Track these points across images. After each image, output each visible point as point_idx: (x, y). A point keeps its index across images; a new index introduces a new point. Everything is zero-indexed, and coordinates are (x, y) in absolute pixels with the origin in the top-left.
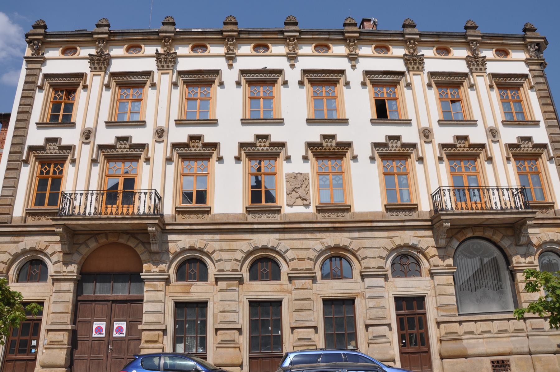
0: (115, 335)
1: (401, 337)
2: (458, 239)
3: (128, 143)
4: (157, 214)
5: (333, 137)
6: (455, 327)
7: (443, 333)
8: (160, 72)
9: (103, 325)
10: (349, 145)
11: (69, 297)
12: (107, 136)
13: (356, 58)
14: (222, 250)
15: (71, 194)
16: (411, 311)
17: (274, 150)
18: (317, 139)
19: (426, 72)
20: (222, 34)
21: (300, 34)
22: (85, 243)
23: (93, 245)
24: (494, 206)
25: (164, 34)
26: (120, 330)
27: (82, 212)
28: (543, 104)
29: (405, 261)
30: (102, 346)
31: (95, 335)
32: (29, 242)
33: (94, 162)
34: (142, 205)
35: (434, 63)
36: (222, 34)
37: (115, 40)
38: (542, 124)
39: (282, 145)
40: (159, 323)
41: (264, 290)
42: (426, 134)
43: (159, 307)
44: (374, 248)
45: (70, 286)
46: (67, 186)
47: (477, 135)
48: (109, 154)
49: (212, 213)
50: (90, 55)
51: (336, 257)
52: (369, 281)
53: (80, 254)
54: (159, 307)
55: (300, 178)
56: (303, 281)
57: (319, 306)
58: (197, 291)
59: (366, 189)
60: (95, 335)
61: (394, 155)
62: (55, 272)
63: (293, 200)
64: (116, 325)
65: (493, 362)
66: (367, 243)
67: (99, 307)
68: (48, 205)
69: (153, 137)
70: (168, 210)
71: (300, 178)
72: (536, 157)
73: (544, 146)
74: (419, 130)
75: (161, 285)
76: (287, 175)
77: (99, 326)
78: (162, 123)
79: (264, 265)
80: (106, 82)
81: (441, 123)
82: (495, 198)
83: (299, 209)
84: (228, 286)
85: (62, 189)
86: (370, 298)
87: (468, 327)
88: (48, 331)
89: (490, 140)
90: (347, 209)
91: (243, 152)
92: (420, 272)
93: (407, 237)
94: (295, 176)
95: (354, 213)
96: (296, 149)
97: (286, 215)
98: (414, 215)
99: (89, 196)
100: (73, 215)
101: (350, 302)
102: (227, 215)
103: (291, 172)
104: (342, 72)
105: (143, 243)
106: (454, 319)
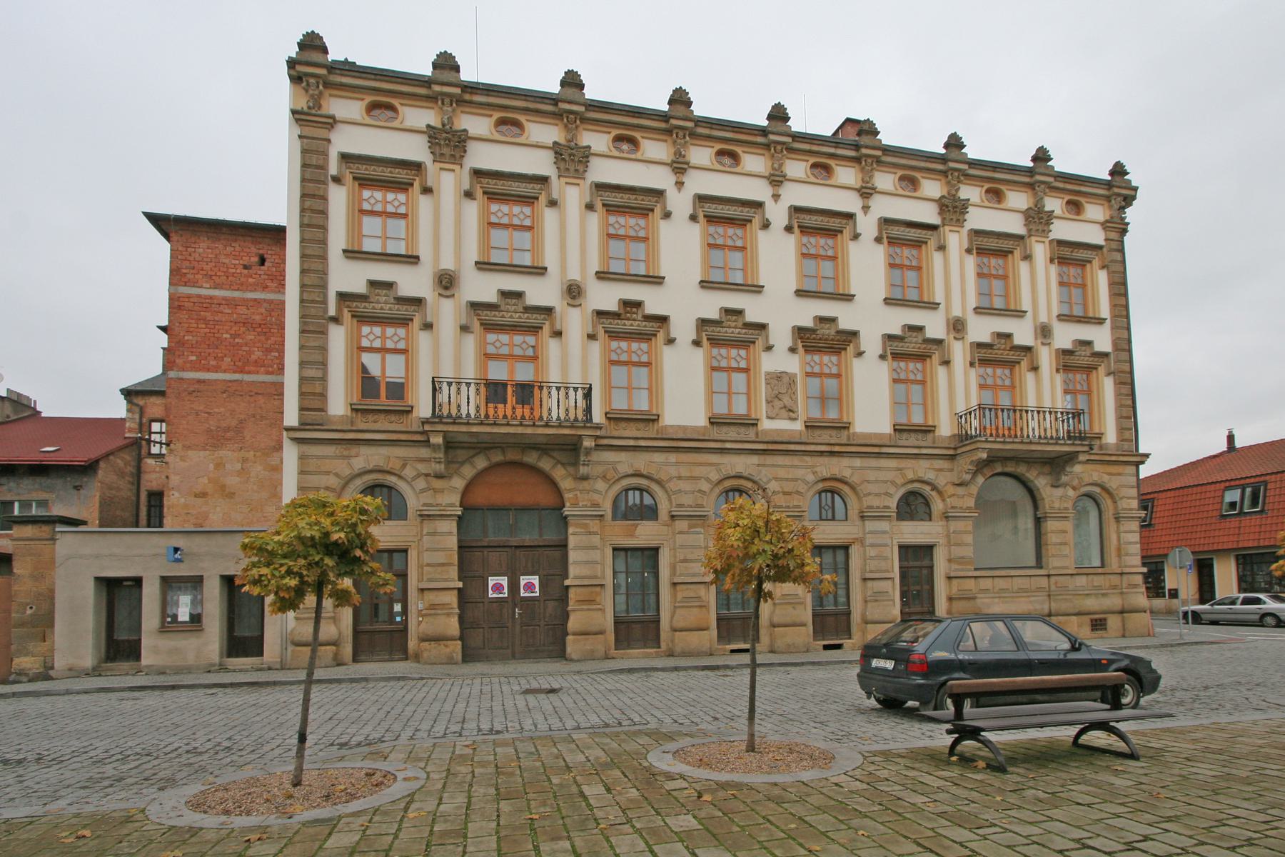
0: (523, 594)
1: (903, 594)
2: (984, 475)
3: (392, 294)
5: (833, 320)
6: (970, 584)
7: (955, 590)
8: (563, 180)
9: (504, 581)
10: (854, 334)
11: (453, 542)
13: (685, 170)
16: (916, 559)
18: (808, 323)
19: (589, 182)
20: (556, 105)
21: (330, 72)
22: (469, 460)
23: (481, 463)
24: (545, 415)
25: (567, 106)
26: (530, 587)
27: (562, 416)
28: (1115, 294)
29: (913, 504)
30: (505, 611)
31: (491, 595)
32: (366, 458)
34: (554, 407)
35: (982, 218)
36: (667, 121)
37: (471, 102)
38: (1108, 322)
39: (762, 327)
41: (915, 532)
42: (957, 326)
44: (882, 482)
45: (451, 526)
47: (1023, 334)
49: (661, 423)
50: (428, 126)
51: (634, 489)
52: (870, 525)
53: (463, 477)
55: (786, 380)
58: (645, 533)
59: (872, 403)
60: (491, 595)
61: (910, 351)
63: (776, 410)
64: (524, 580)
66: (872, 475)
67: (494, 557)
72: (1089, 369)
73: (1106, 355)
74: (948, 320)
75: (594, 525)
76: (767, 374)
77: (497, 585)
80: (966, 246)
81: (978, 310)
82: (1033, 424)
83: (783, 425)
84: (690, 527)
86: (872, 545)
87: (986, 584)
89: (1039, 341)
90: (651, 419)
91: (346, 310)
92: (930, 515)
93: (923, 469)
94: (779, 376)
95: (854, 434)
96: (781, 336)
97: (766, 432)
98: (651, 431)
100: (998, 436)
102: (685, 428)
103: (771, 369)
104: (659, 193)
106: (970, 574)
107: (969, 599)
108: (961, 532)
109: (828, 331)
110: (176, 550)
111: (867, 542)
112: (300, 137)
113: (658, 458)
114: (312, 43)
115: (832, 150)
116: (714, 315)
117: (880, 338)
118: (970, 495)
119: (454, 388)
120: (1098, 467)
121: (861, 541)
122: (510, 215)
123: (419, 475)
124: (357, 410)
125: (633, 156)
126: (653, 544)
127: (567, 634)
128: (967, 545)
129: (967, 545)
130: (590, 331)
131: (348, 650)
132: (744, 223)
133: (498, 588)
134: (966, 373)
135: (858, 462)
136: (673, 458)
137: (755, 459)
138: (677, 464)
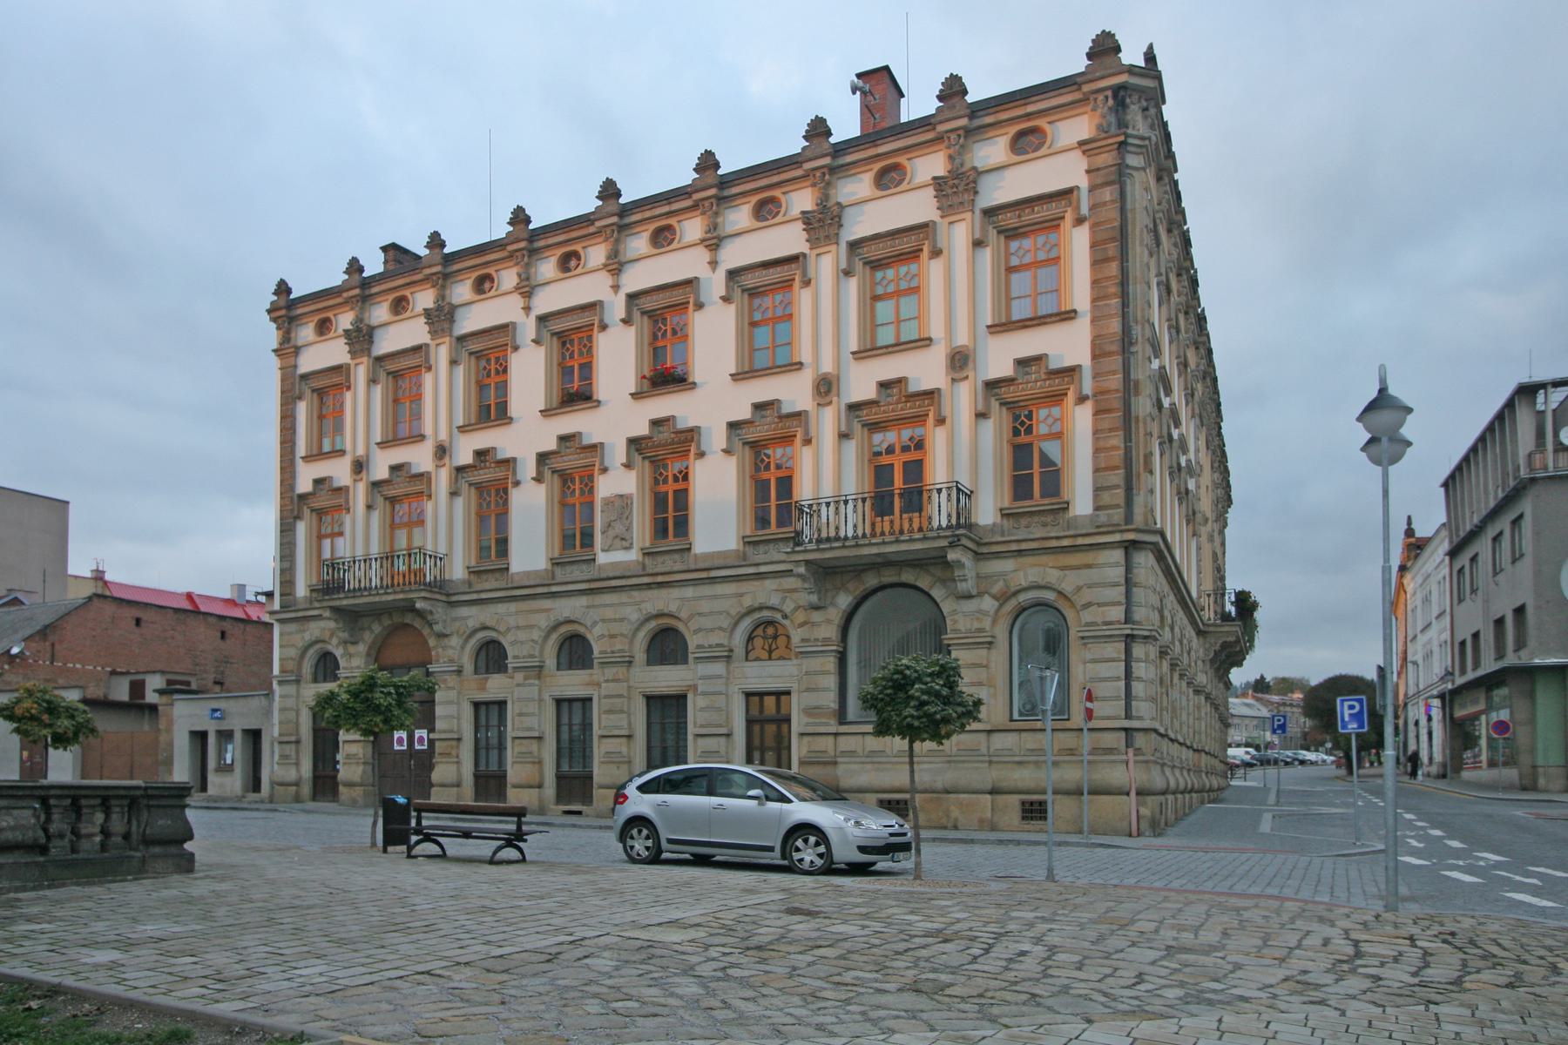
0: (417, 747)
4: (963, 526)
9: (404, 735)
12: (861, 383)
14: (518, 628)
15: (810, 506)
17: (1056, 385)
29: (767, 634)
31: (397, 747)
33: (843, 436)
40: (451, 731)
41: (667, 679)
43: (452, 710)
46: (804, 491)
48: (864, 417)
54: (452, 710)
56: (614, 670)
57: (640, 707)
58: (496, 686)
60: (397, 747)
62: (803, 640)
65: (1023, 803)
66: (705, 606)
68: (1042, 497)
69: (947, 374)
70: (986, 513)
71: (618, 503)
78: (962, 339)
79: (667, 644)
80: (843, 265)
83: (619, 556)
84: (526, 678)
85: (795, 498)
86: (704, 694)
88: (802, 734)
99: (842, 506)
100: (873, 535)
101: (679, 700)
105: (943, 582)
107: (825, 763)
108: (816, 673)
109: (665, 435)
110: (215, 710)
111: (700, 689)
112: (1088, 172)
113: (501, 608)
114: (283, 288)
115: (666, 209)
116: (745, 413)
117: (724, 426)
118: (829, 621)
119: (832, 508)
120: (1044, 559)
121: (695, 687)
122: (898, 279)
123: (797, 608)
124: (1008, 515)
125: (776, 220)
126: (500, 697)
127: (432, 785)
128: (825, 690)
129: (825, 690)
130: (980, 408)
131: (306, 789)
132: (914, 255)
133: (400, 740)
134: (839, 452)
135: (689, 592)
136: (513, 607)
137: (584, 601)
138: (517, 613)
